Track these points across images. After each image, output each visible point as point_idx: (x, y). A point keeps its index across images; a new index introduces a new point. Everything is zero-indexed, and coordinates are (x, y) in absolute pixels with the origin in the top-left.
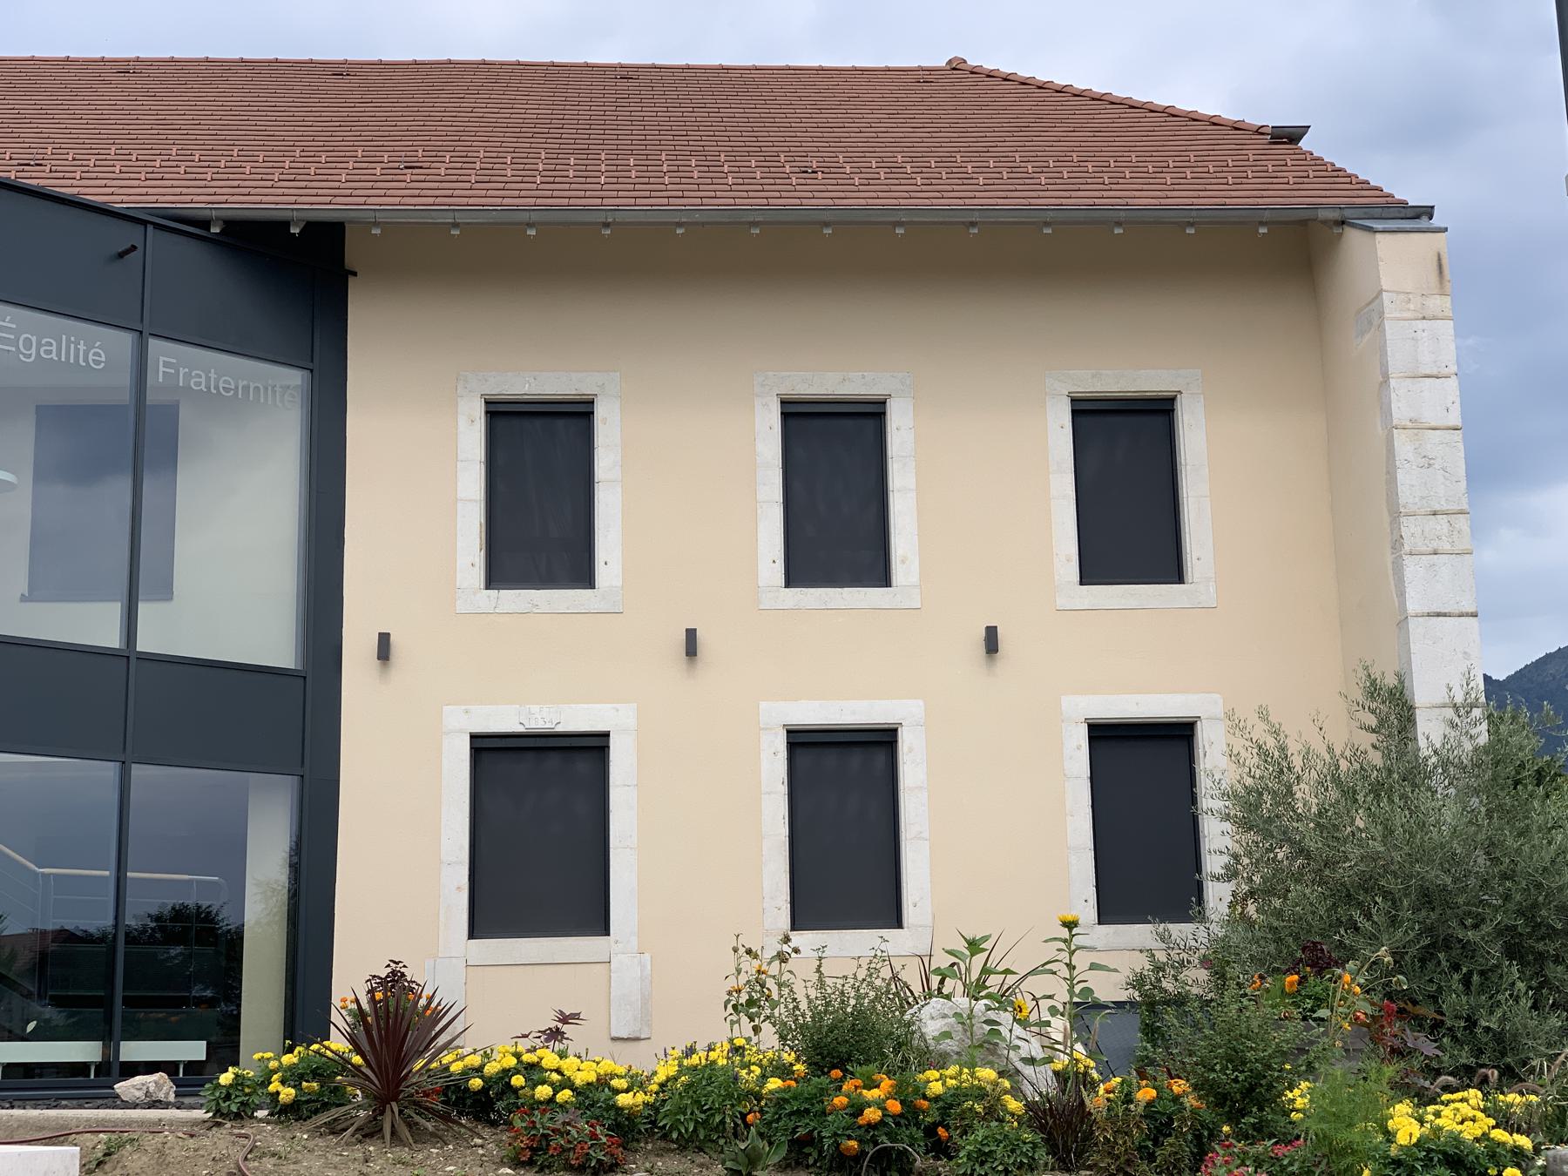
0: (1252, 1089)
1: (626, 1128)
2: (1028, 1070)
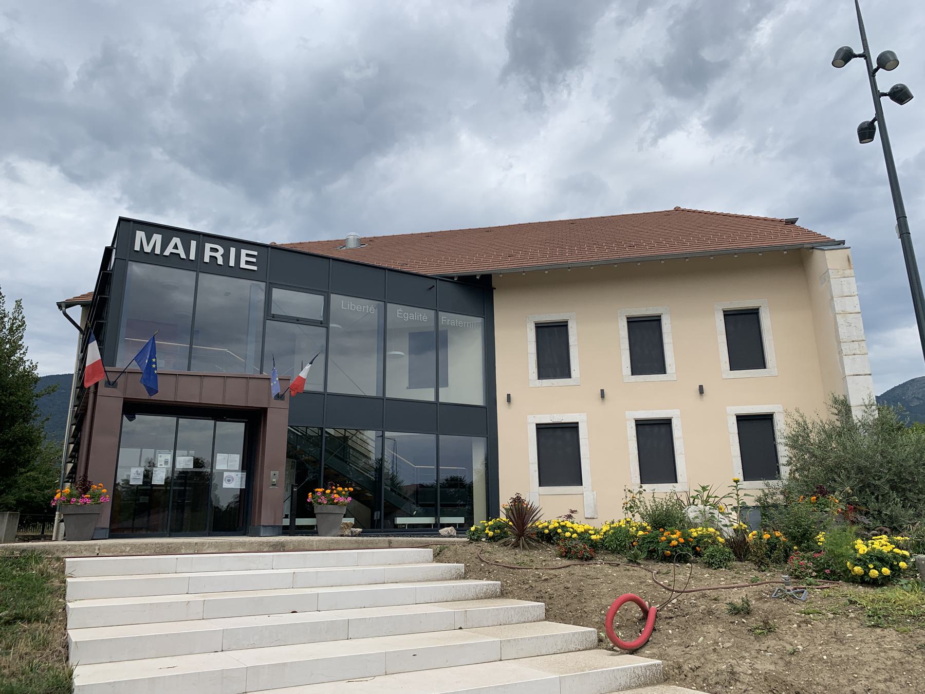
0: (804, 534)
1: (594, 546)
2: (725, 529)
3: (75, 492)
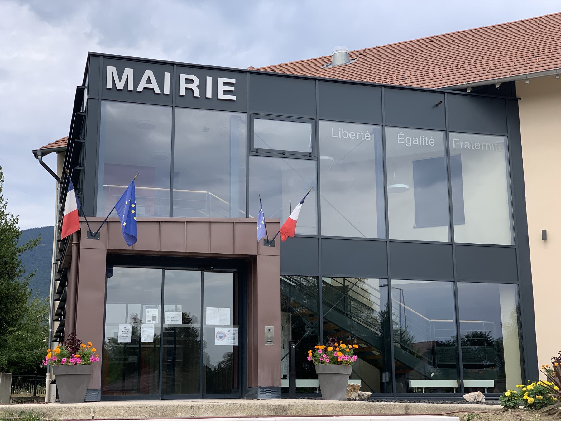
3: (65, 352)
